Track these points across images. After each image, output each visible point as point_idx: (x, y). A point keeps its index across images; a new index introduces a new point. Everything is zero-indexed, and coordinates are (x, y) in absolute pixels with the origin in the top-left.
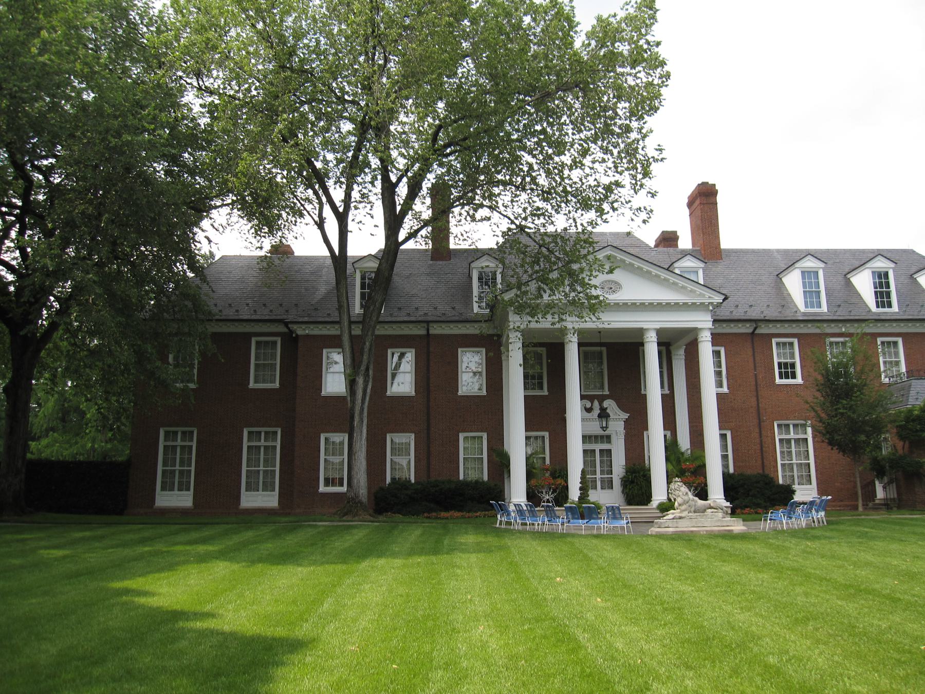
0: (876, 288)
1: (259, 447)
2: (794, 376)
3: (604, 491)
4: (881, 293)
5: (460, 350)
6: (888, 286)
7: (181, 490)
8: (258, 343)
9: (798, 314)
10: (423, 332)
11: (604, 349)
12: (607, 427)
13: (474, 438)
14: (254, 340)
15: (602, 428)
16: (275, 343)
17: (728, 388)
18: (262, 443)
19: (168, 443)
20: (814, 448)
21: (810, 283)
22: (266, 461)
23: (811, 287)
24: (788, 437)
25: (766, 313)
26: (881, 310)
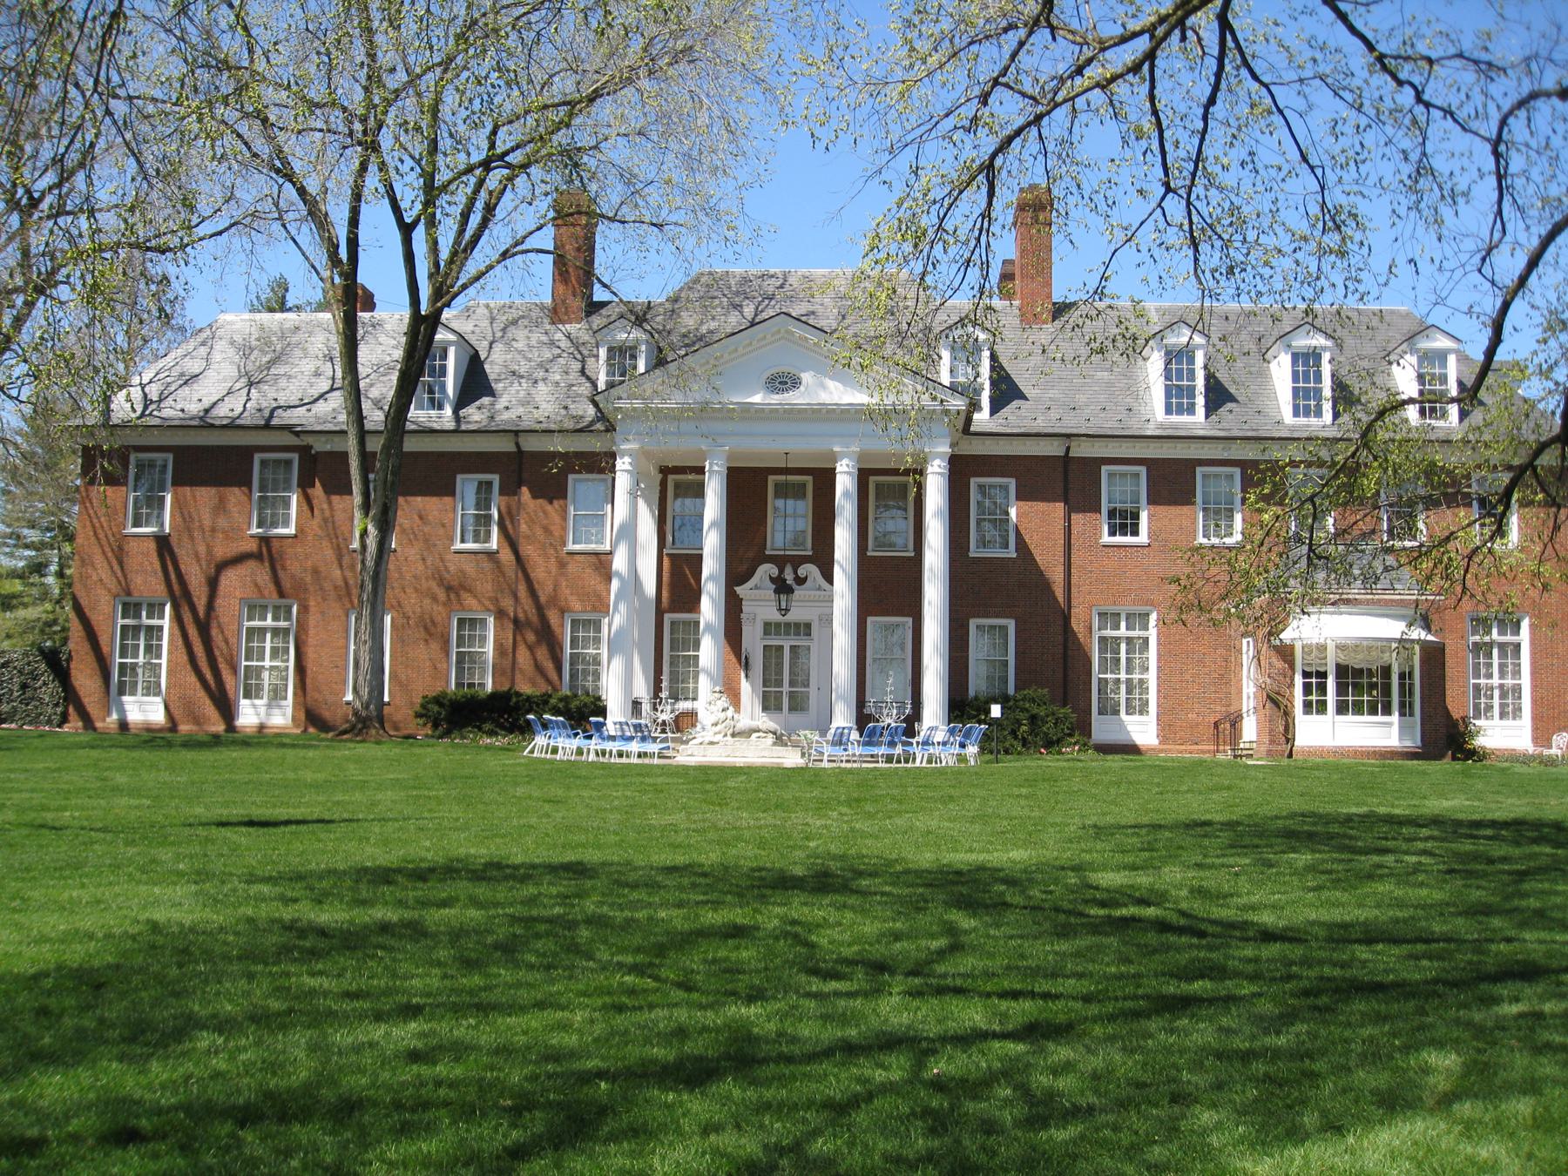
0: (1167, 378)
1: (1491, 645)
2: (1135, 533)
3: (1505, 722)
4: (1306, 390)
5: (459, 477)
6: (1318, 378)
7: (148, 695)
8: (263, 463)
9: (1151, 425)
10: (511, 448)
11: (809, 479)
12: (787, 610)
13: (992, 627)
14: (257, 457)
15: (780, 609)
16: (288, 463)
17: (1017, 550)
18: (1123, 631)
19: (128, 622)
20: (1159, 655)
21: (1180, 372)
22: (1502, 667)
23: (1307, 380)
24: (1487, 639)
25: (1065, 422)
26: (1302, 420)
